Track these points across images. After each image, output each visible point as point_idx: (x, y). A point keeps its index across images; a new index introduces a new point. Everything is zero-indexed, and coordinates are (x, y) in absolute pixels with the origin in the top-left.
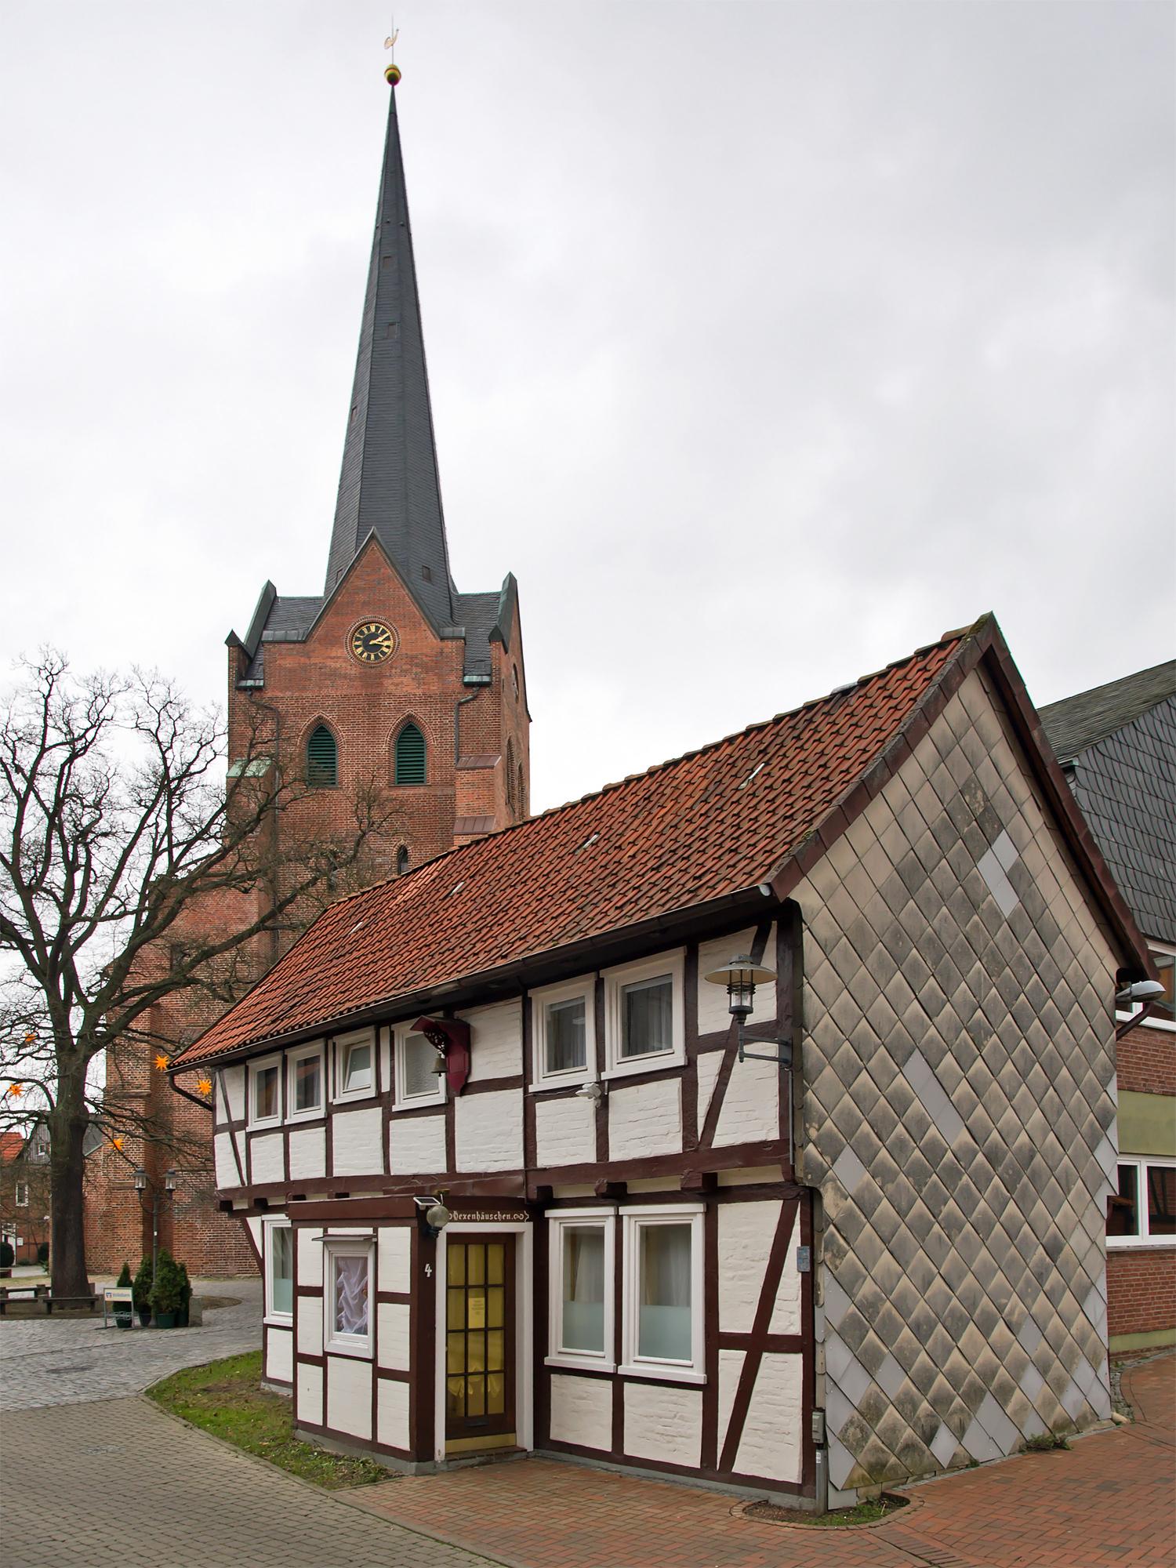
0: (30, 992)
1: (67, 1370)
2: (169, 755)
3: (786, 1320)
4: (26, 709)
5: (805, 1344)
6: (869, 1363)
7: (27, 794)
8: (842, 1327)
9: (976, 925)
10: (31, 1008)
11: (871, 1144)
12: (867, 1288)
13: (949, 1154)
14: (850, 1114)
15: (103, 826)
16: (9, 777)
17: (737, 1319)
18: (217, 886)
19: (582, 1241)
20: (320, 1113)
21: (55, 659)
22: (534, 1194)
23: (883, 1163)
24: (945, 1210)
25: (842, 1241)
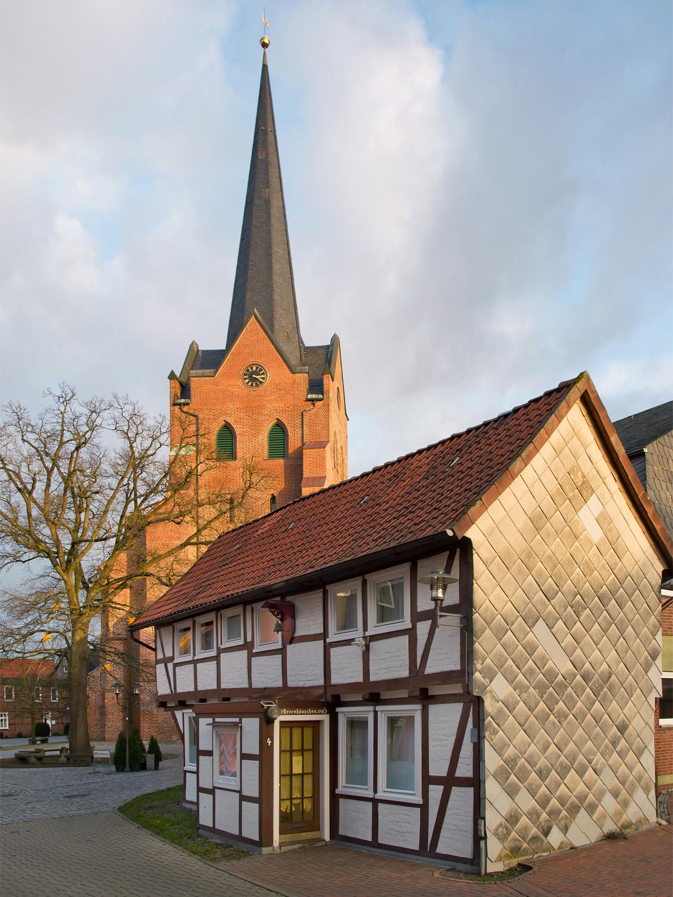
0: (55, 582)
1: (75, 796)
2: (134, 445)
3: (465, 769)
4: (51, 420)
5: (476, 782)
6: (512, 792)
7: (52, 469)
8: (495, 773)
9: (577, 548)
10: (56, 591)
11: (513, 672)
12: (510, 751)
13: (560, 676)
14: (501, 655)
15: (95, 488)
16: (42, 459)
17: (439, 768)
18: (163, 520)
19: (357, 725)
20: (213, 653)
21: (68, 391)
22: (330, 699)
23: (520, 682)
24: (557, 707)
25: (495, 726)
